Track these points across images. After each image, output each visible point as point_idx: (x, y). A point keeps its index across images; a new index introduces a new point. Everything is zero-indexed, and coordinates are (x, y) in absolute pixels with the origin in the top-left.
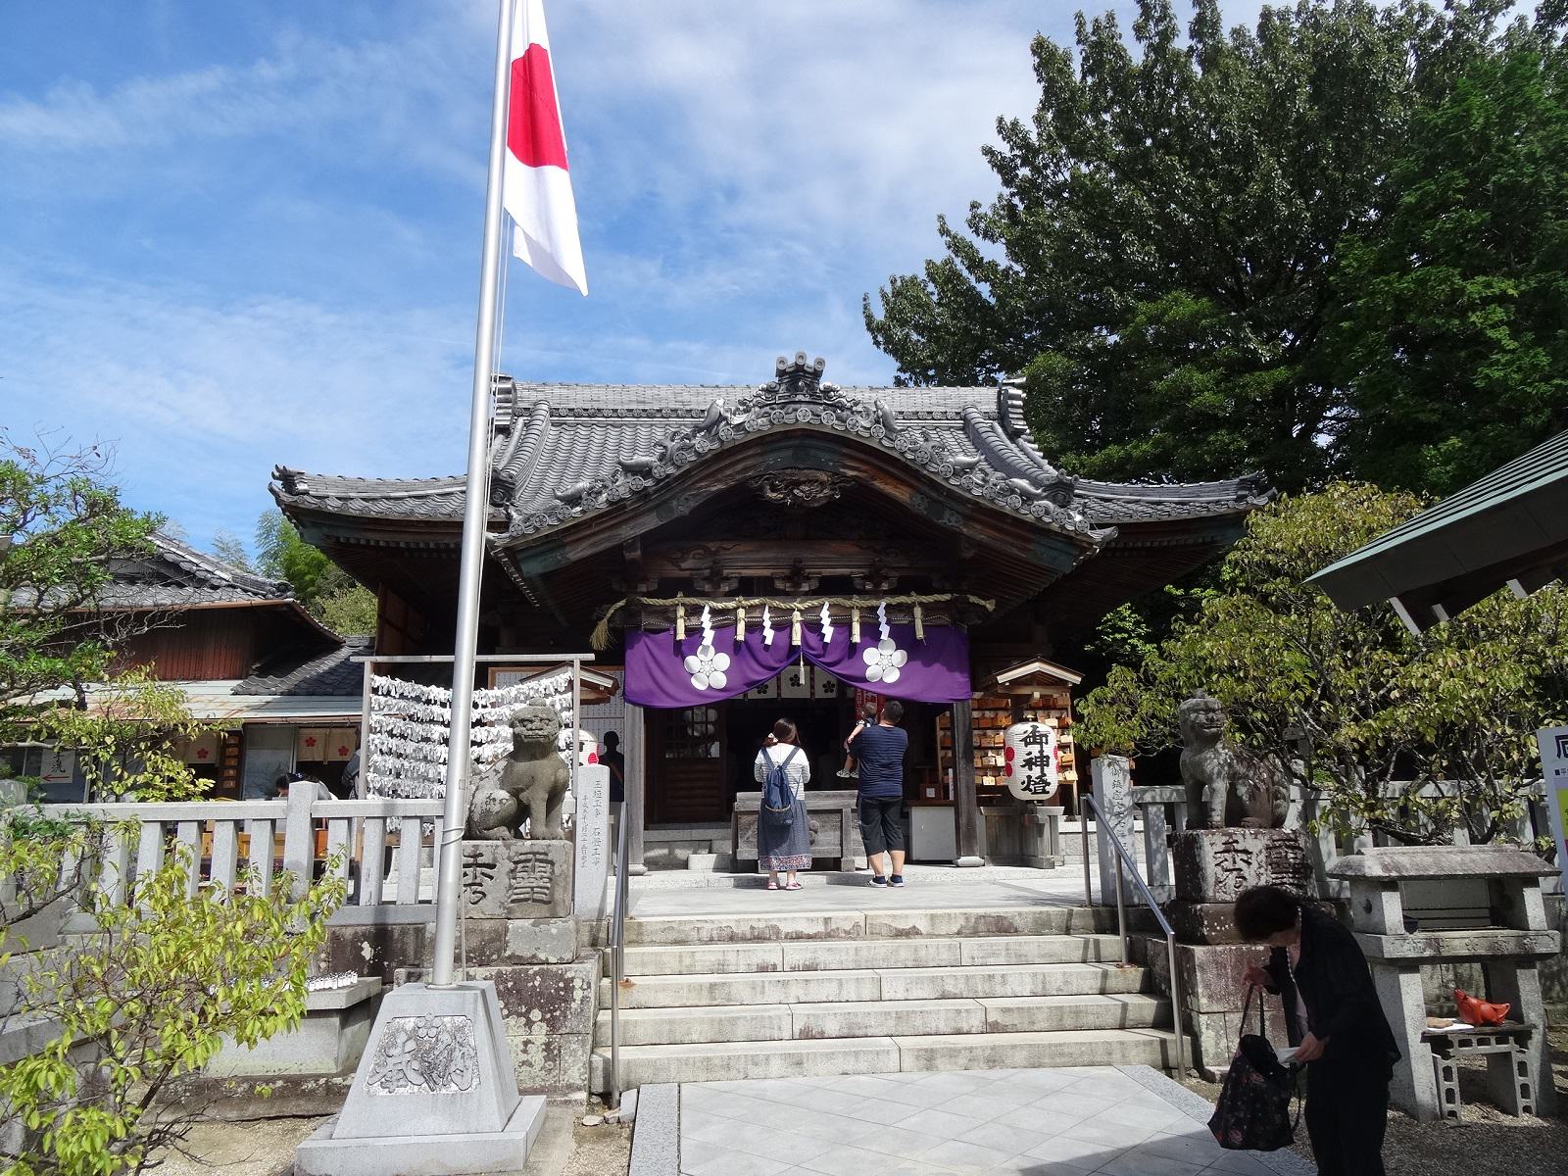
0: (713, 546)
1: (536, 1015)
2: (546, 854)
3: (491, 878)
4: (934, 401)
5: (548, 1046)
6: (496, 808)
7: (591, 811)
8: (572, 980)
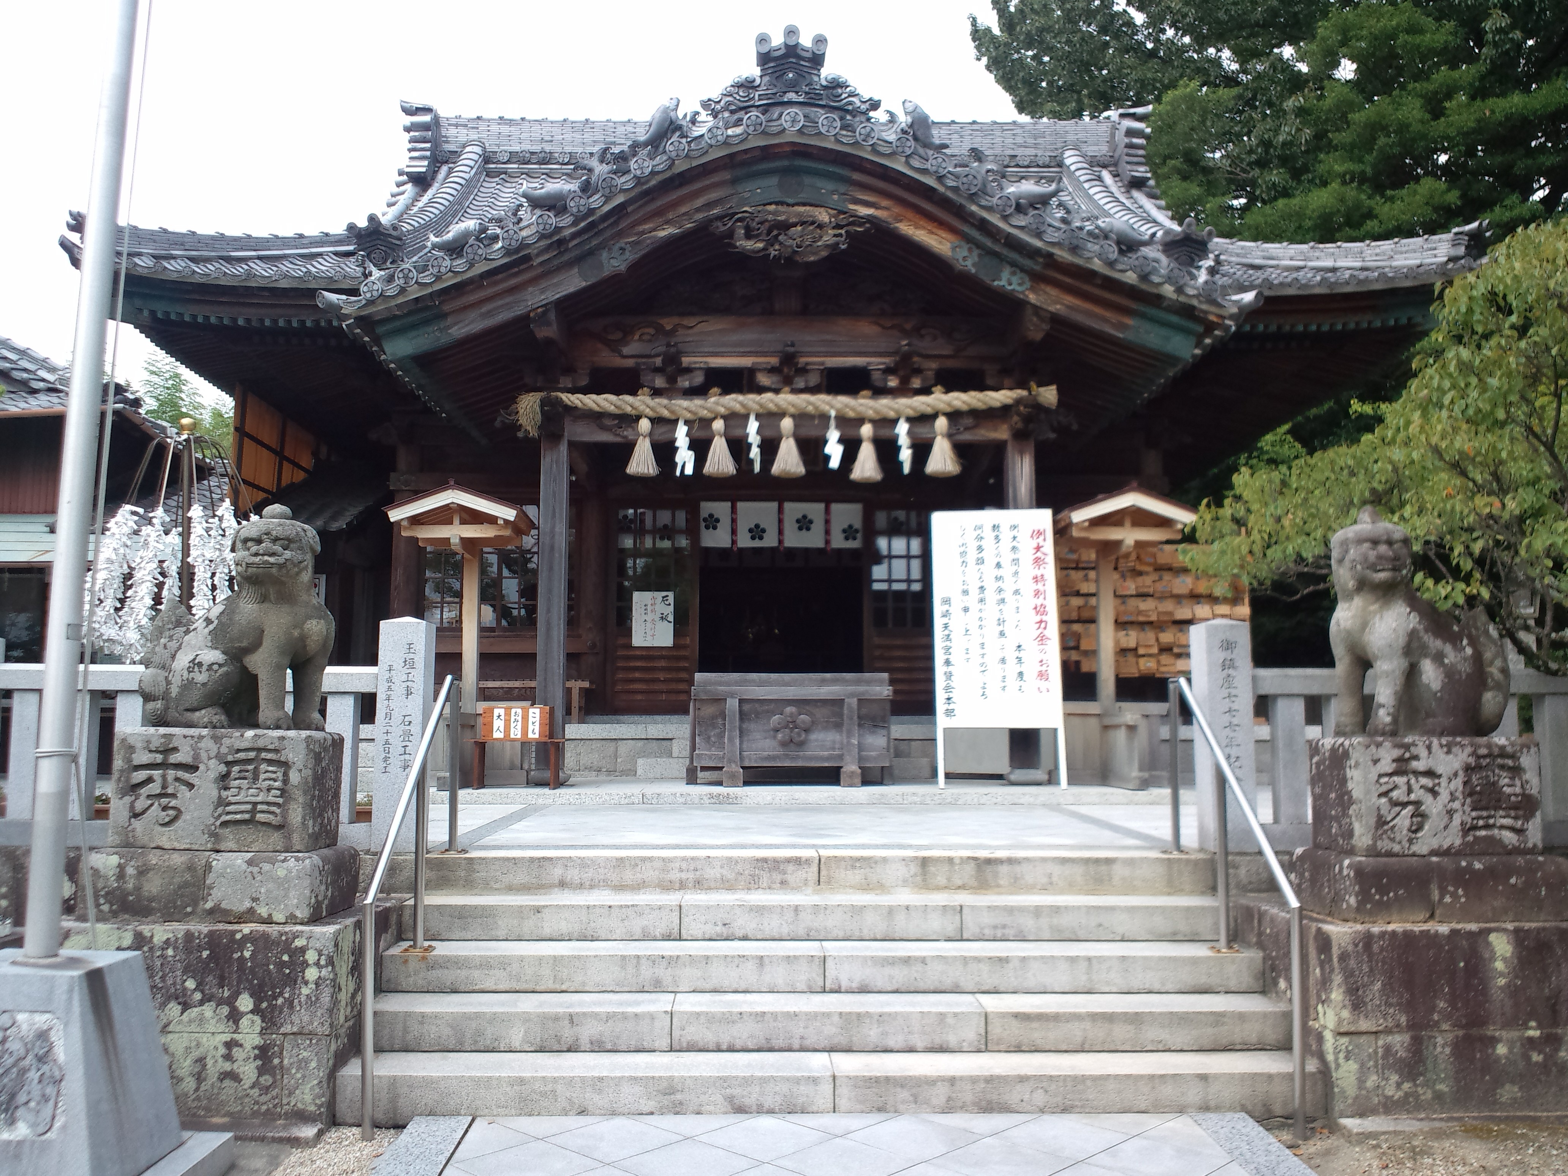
0: (668, 323)
1: (245, 1003)
2: (276, 751)
3: (191, 786)
4: (1019, 140)
5: (264, 1053)
6: (201, 677)
7: (399, 689)
8: (303, 950)
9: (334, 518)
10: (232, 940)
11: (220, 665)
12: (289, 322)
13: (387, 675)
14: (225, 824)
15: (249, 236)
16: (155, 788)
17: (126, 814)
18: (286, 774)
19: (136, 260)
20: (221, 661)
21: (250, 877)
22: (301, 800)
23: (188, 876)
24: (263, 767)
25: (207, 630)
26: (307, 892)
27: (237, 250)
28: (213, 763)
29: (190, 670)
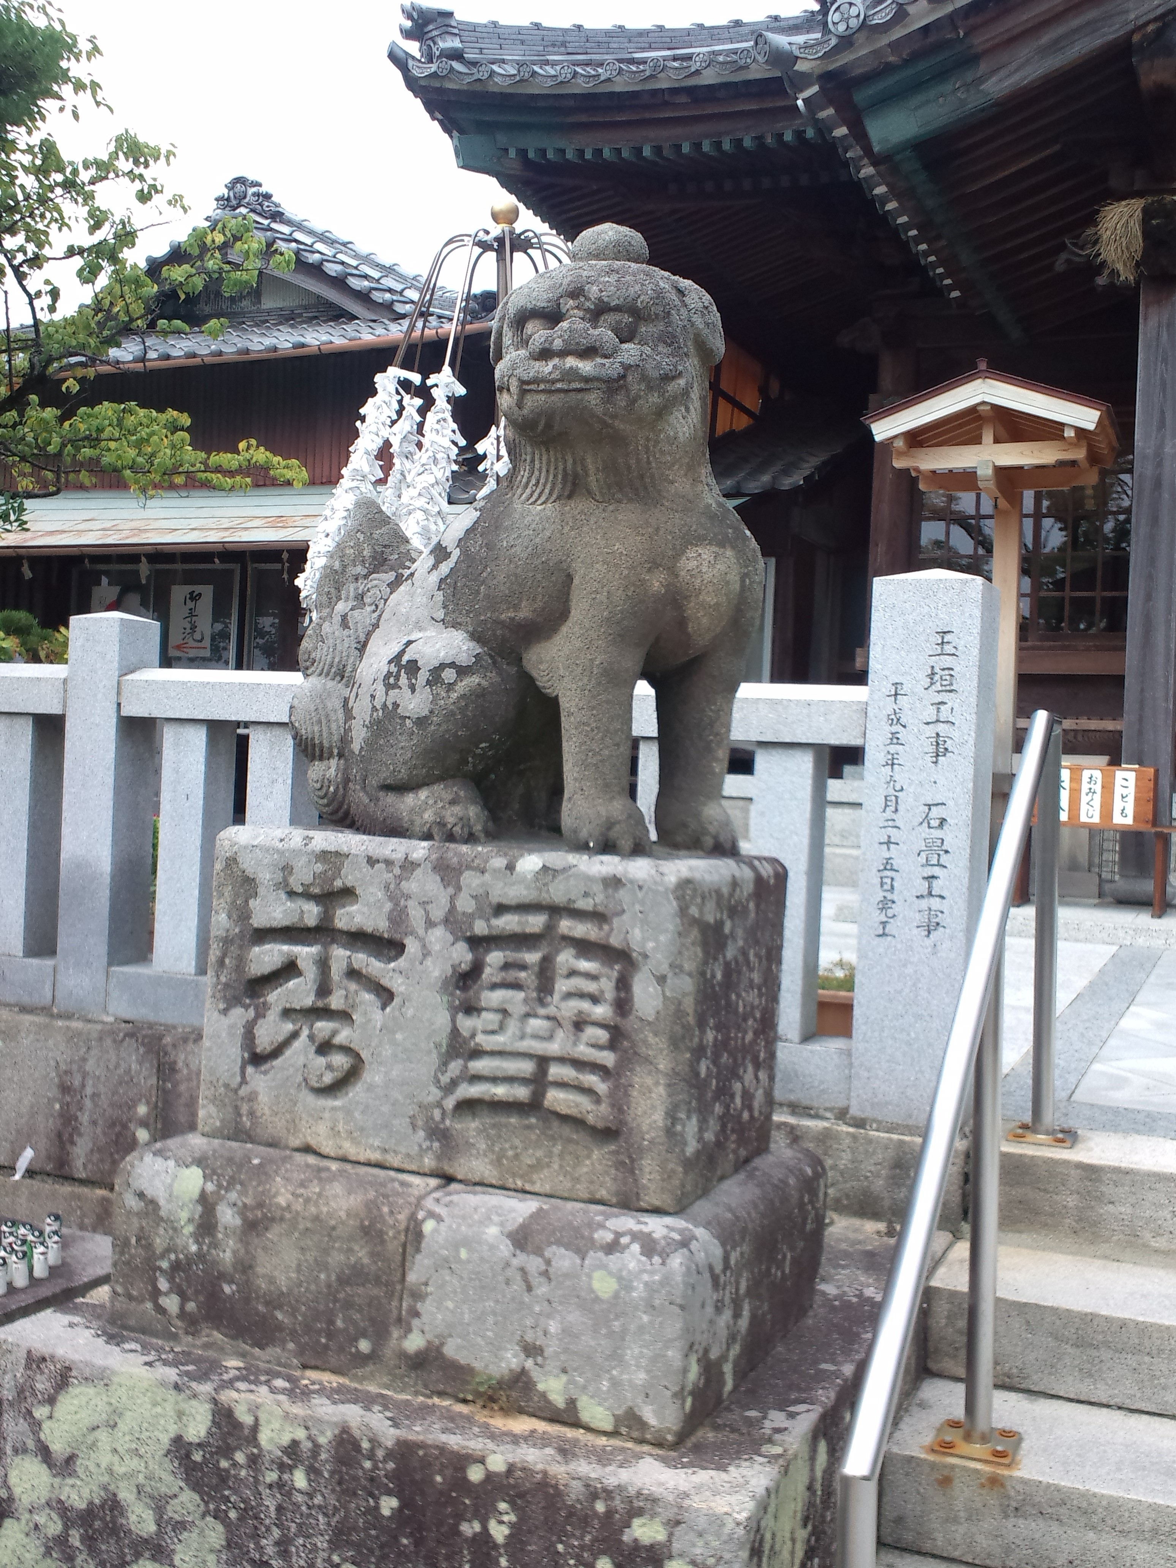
2: (598, 917)
3: (386, 995)
6: (414, 702)
7: (917, 740)
9: (786, 472)
10: (462, 1483)
11: (462, 671)
12: (718, 145)
13: (889, 706)
14: (468, 1106)
15: (661, 28)
16: (299, 991)
17: (235, 1053)
18: (623, 984)
19: (495, 68)
20: (464, 660)
21: (518, 1286)
22: (663, 1064)
23: (362, 1254)
24: (566, 958)
25: (434, 578)
26: (674, 1355)
27: (643, 50)
28: (438, 936)
29: (390, 682)
